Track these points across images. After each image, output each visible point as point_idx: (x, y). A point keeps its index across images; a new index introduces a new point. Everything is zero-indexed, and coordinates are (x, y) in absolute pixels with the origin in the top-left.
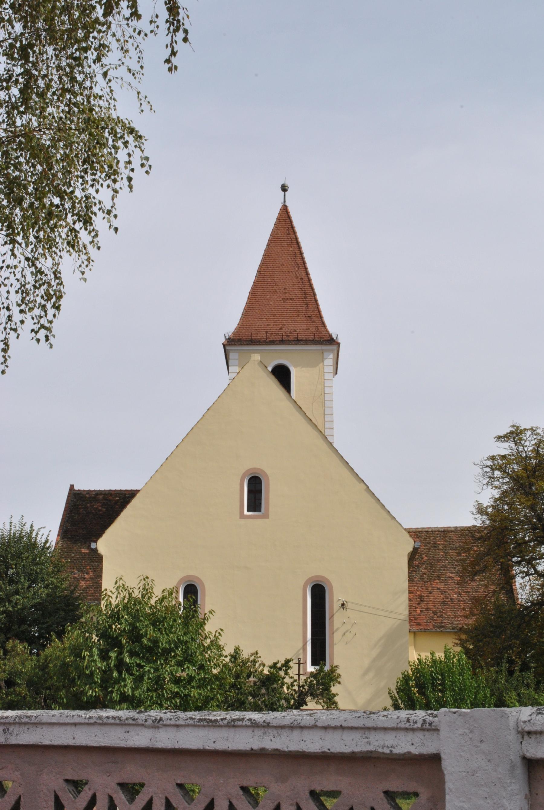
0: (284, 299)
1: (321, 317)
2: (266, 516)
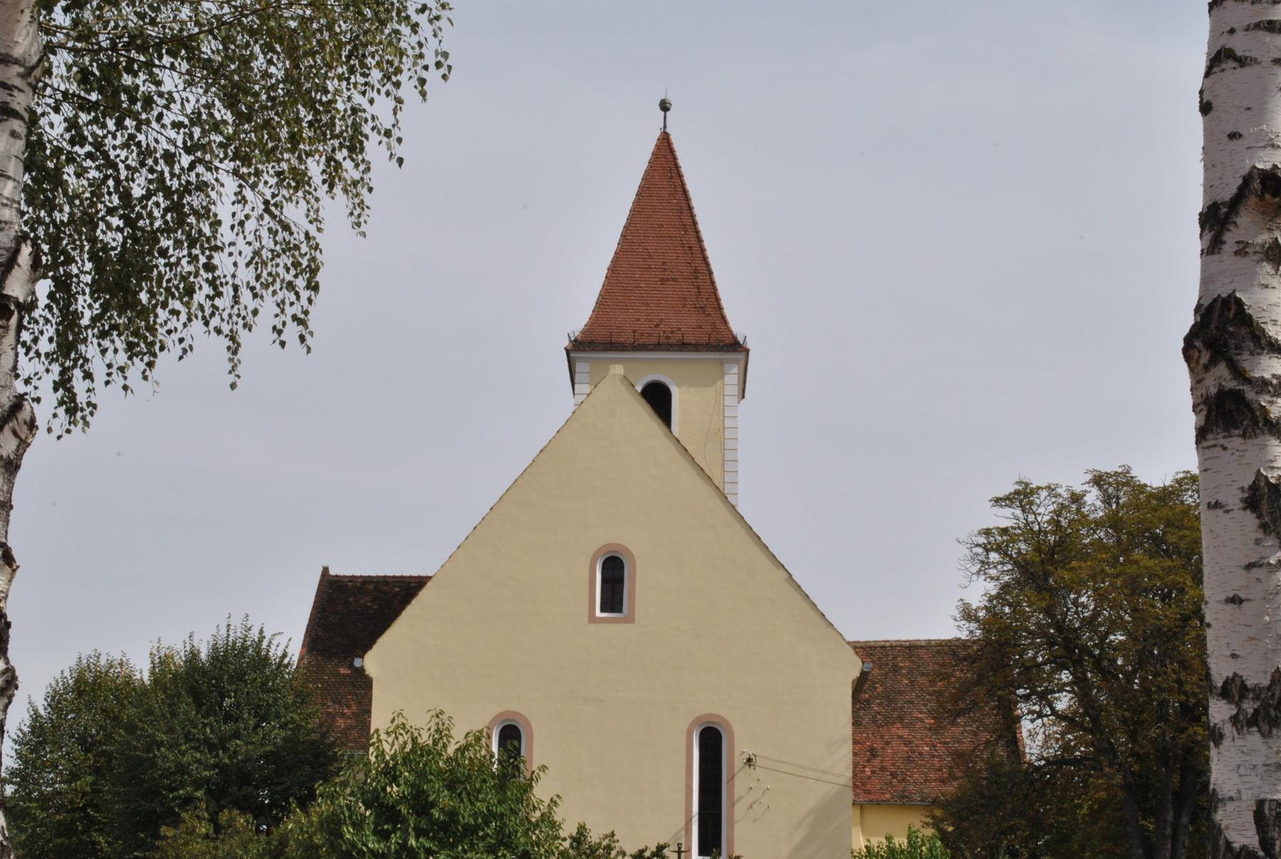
0: (662, 280)
1: (720, 308)
2: (630, 620)
